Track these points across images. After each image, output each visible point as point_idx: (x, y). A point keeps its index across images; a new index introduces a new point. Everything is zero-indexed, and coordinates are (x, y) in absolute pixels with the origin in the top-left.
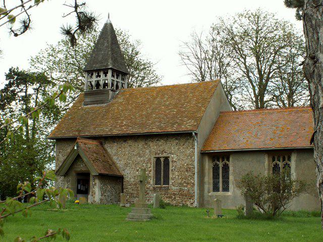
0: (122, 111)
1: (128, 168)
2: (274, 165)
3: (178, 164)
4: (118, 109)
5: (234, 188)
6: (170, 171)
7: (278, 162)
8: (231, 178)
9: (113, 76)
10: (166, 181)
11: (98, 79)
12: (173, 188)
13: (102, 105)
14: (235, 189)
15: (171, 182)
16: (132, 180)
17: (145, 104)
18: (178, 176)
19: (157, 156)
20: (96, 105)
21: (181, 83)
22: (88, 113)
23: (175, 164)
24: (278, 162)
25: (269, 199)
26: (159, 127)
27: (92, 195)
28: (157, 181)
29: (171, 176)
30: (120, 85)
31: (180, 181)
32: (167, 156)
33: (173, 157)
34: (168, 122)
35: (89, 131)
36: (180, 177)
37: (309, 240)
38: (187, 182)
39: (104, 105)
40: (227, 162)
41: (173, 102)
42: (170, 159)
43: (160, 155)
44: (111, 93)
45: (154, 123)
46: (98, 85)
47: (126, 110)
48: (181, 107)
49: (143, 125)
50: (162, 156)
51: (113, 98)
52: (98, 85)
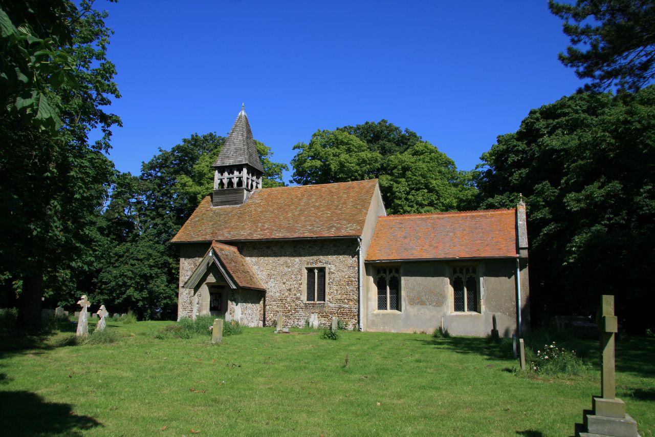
0: (261, 212)
1: (272, 280)
2: (455, 278)
3: (337, 276)
4: (256, 210)
5: (406, 305)
6: (327, 285)
7: (461, 276)
8: (403, 293)
9: (248, 173)
10: (322, 297)
11: (231, 176)
12: (331, 305)
13: (235, 206)
14: (408, 307)
15: (327, 297)
16: (278, 294)
17: (289, 206)
18: (337, 290)
19: (310, 266)
20: (228, 206)
21: (271, 260)
22: (219, 215)
23: (333, 276)
24: (461, 276)
25: (607, 10)
26: (310, 231)
27: (230, 313)
28: (310, 297)
29: (327, 290)
30: (254, 184)
31: (339, 297)
32: (323, 266)
33: (327, 267)
34: (323, 225)
35: (223, 235)
36: (339, 292)
37: (475, 435)
38: (347, 298)
39: (238, 206)
40: (396, 275)
41: (324, 203)
42: (327, 271)
43: (314, 266)
44: (245, 192)
45: (304, 226)
46: (230, 183)
47: (266, 211)
48: (336, 209)
49: (291, 229)
50: (316, 266)
51: (248, 198)
52: (230, 183)
